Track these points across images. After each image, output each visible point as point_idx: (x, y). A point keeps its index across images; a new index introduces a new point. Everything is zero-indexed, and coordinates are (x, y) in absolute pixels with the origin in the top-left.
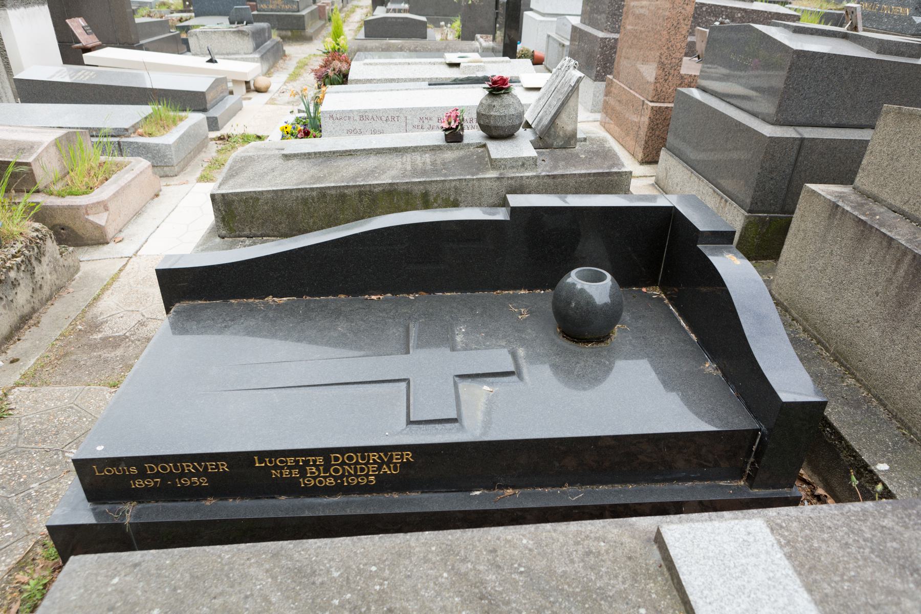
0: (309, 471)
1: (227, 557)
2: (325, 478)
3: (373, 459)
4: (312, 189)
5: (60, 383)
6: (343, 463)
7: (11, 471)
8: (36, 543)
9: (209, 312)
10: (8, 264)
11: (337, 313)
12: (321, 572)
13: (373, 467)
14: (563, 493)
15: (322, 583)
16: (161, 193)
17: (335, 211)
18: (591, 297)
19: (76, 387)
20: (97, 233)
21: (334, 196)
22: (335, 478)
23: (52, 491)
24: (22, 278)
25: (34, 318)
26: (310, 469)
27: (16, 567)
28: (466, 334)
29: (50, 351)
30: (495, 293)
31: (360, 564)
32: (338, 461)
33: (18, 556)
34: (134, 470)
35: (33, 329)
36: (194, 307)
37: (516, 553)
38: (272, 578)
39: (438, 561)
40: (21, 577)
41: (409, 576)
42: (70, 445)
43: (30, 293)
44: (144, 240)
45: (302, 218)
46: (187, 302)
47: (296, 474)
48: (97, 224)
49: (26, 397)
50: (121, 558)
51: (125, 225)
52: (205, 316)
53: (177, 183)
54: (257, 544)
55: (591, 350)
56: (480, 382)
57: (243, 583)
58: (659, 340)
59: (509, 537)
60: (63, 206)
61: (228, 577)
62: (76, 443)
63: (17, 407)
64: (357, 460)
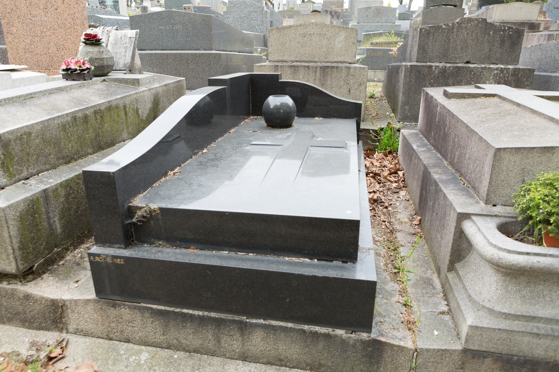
4: (67, 114)
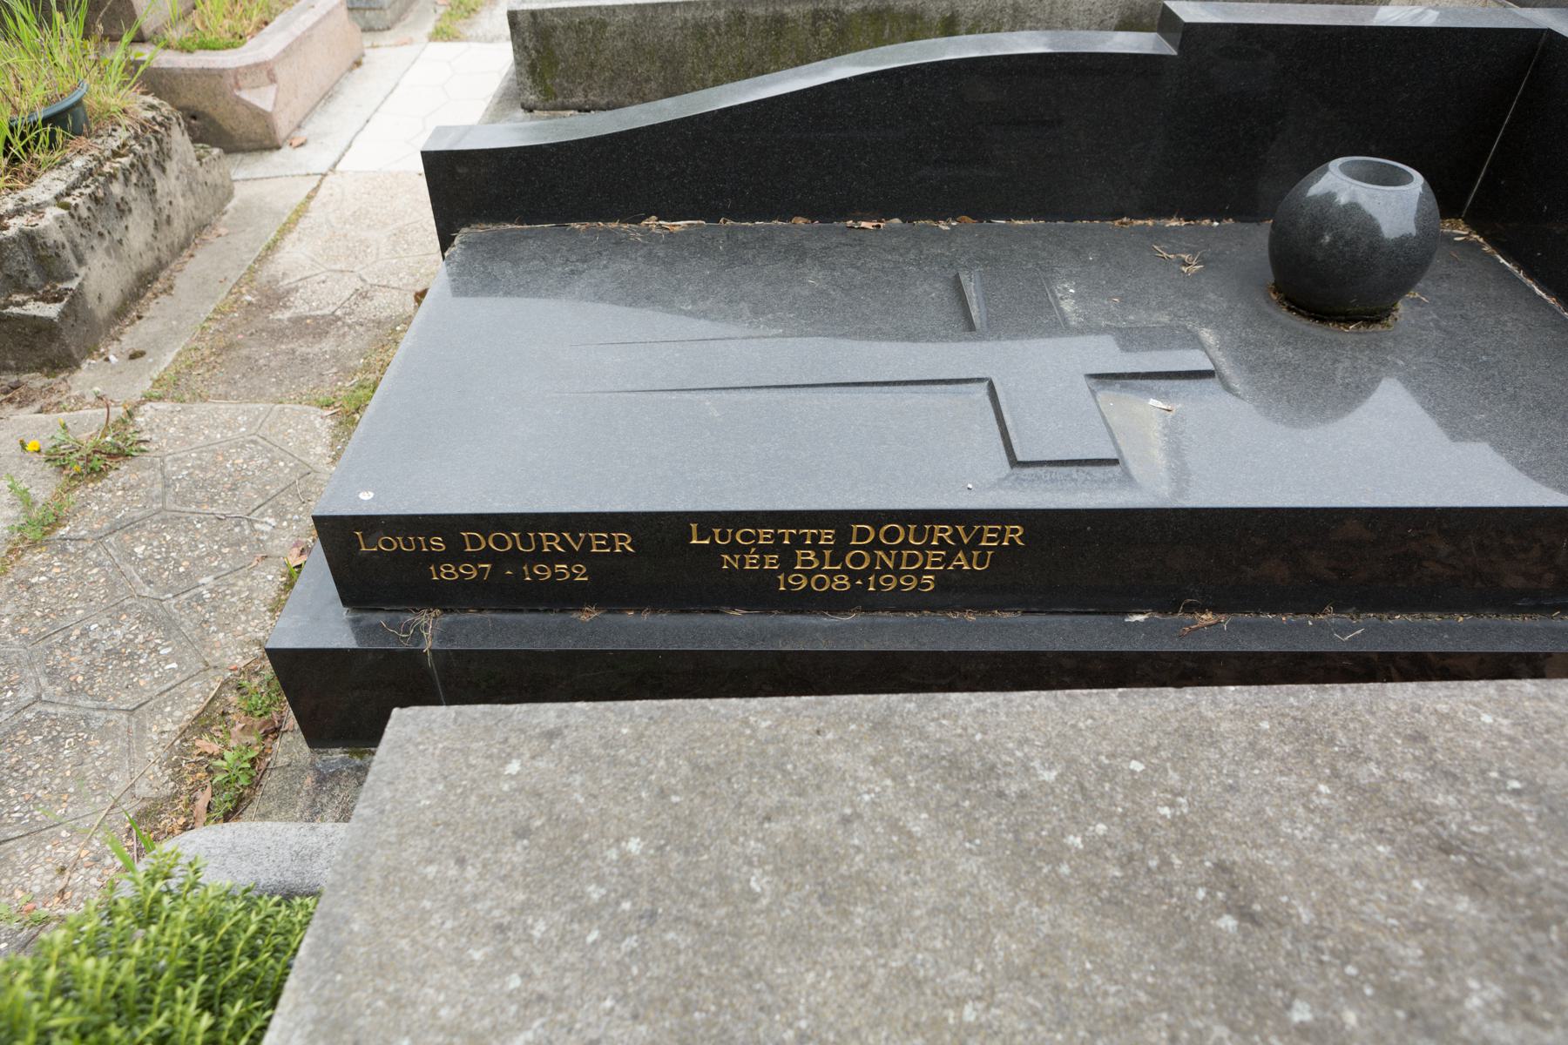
0: (800, 558)
1: (764, 725)
2: (831, 574)
3: (941, 539)
5: (226, 398)
6: (876, 544)
7: (159, 553)
8: (225, 683)
9: (533, 245)
10: (107, 168)
11: (798, 253)
12: (1011, 770)
13: (935, 556)
14: (1319, 624)
15: (1022, 795)
16: (364, 60)
17: (761, 55)
18: (1371, 218)
19: (258, 406)
20: (258, 128)
21: (761, 21)
22: (853, 576)
23: (239, 592)
24: (135, 200)
25: (161, 279)
26: (803, 555)
27: (193, 726)
28: (1078, 297)
29: (199, 339)
30: (1116, 223)
31: (1099, 753)
32: (886, 538)
33: (194, 706)
34: (438, 543)
35: (163, 298)
36: (500, 236)
37: (1479, 744)
38: (894, 779)
39: (1289, 755)
40: (206, 744)
41: (1232, 789)
42: (262, 509)
43: (150, 230)
44: (345, 144)
45: (692, 68)
46: (484, 226)
47: (772, 564)
48: (257, 108)
49: (167, 420)
50: (511, 716)
51: (307, 115)
52: (526, 253)
53: (392, 42)
54: (828, 698)
55: (1357, 338)
56: (1140, 390)
57: (826, 787)
58: (1498, 322)
59: (1443, 708)
60: (192, 70)
61: (785, 773)
62: (272, 507)
63: (154, 439)
64: (906, 538)
